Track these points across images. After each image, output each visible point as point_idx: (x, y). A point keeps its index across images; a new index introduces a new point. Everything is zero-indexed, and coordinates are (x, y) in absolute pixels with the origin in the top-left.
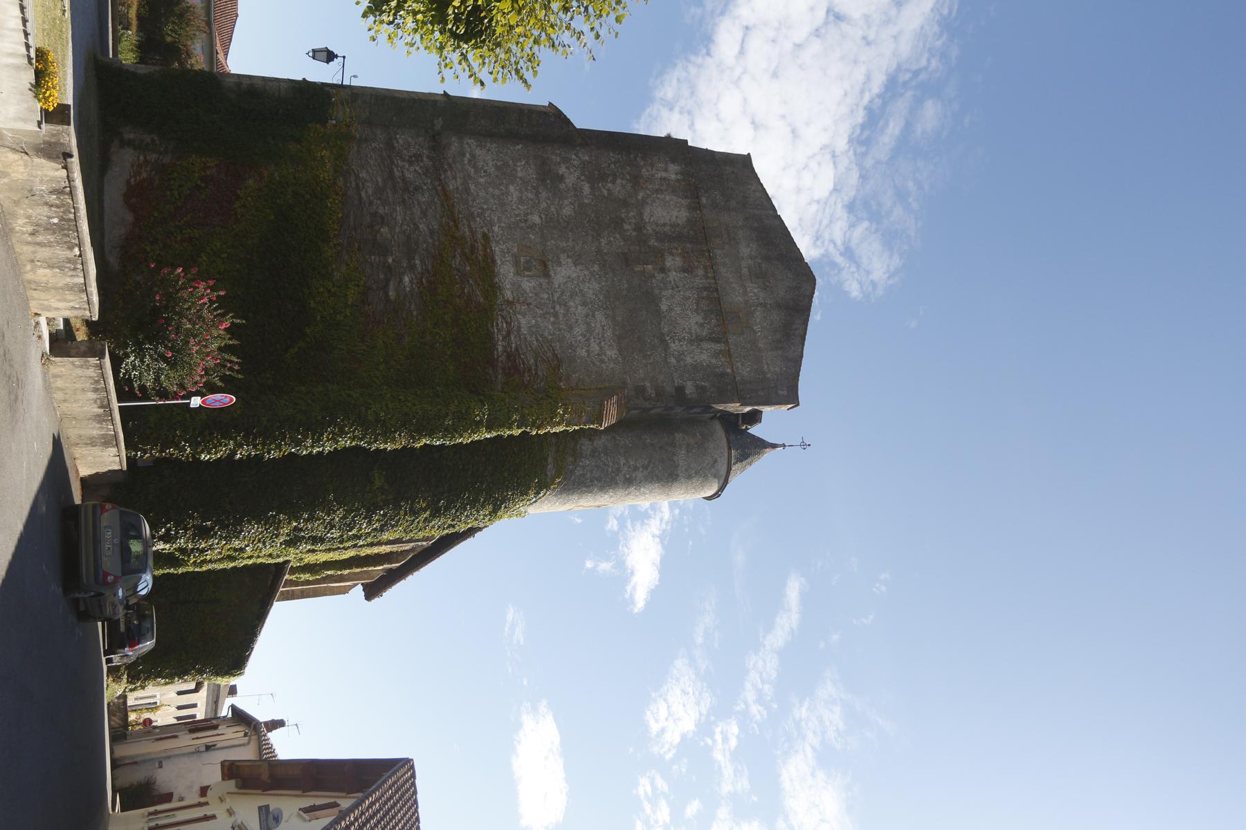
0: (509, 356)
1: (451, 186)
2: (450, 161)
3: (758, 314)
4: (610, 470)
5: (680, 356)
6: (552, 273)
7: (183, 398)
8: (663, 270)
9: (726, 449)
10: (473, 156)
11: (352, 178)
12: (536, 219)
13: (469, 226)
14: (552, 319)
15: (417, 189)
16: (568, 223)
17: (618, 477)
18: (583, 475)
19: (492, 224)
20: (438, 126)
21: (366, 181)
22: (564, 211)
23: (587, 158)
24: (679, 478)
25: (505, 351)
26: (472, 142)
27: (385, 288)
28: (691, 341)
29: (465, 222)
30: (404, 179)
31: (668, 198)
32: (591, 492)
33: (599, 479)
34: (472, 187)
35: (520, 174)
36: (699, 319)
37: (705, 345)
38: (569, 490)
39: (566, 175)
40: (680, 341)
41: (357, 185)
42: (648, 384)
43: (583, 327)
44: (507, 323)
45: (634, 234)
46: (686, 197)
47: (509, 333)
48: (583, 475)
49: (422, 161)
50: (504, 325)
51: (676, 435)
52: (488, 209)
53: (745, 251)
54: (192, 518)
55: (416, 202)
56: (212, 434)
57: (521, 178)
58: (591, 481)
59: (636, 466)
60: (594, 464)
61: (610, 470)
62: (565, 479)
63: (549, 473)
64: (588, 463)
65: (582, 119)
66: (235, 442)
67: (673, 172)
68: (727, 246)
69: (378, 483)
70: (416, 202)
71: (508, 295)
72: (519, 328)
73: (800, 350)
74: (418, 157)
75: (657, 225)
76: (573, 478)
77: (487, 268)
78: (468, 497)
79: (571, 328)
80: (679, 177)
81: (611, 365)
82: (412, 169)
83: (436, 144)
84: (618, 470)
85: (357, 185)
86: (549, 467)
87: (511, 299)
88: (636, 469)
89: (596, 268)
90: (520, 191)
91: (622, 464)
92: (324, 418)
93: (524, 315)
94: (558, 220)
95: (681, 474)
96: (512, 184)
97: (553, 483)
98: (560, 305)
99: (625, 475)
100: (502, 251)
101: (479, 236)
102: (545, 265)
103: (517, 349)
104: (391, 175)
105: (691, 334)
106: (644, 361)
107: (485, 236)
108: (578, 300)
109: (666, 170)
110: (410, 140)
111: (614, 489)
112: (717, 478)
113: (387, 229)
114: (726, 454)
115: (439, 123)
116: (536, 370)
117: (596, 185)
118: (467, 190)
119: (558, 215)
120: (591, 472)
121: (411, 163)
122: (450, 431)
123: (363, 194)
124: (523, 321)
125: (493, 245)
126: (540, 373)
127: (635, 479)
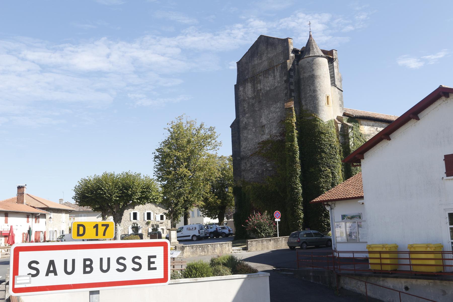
0: (281, 136)
1: (250, 154)
2: (245, 154)
3: (269, 55)
4: (311, 98)
5: (278, 82)
6: (264, 124)
7: (276, 224)
8: (261, 90)
9: (304, 59)
10: (244, 148)
11: (251, 180)
12: (254, 129)
13: (257, 148)
14: (273, 123)
15: (251, 163)
16: (254, 120)
17: (313, 95)
18: (312, 107)
19: (256, 142)
20: (239, 158)
21: (251, 176)
22: (252, 121)
23: (241, 116)
24: (313, 74)
25: (280, 137)
26: (242, 148)
27: (270, 171)
28: (275, 79)
29: (256, 150)
30: (250, 167)
31: (246, 90)
32: (318, 103)
33: (314, 101)
34: (250, 148)
35: (246, 135)
36: (270, 77)
37: (275, 74)
38: (317, 110)
39: (245, 121)
40: (275, 83)
41: (252, 179)
42: (285, 92)
43: (274, 114)
44: (274, 137)
45: (254, 100)
46: (246, 84)
47: (276, 136)
48: (312, 107)
49: (246, 162)
50: (275, 137)
51: (301, 78)
52: (253, 144)
53: (256, 62)
54: (321, 218)
55: (254, 163)
56: (295, 215)
57: (247, 135)
58: (314, 104)
59: (309, 90)
60: (309, 104)
61: (311, 98)
62: (313, 113)
63: (312, 118)
64: (309, 106)
65: (232, 117)
66: (297, 209)
67: (241, 89)
68: (256, 68)
69: (313, 170)
70: (254, 163)
71: (269, 136)
72: (275, 133)
73: (276, 39)
74: (246, 163)
75: (252, 93)
76: (313, 110)
77: (265, 143)
78: (317, 143)
79: (275, 118)
80: (242, 87)
81: (281, 104)
82: (248, 164)
83: (243, 158)
84: (311, 96)
85: (252, 179)
86: (310, 118)
87: (270, 136)
88: (310, 90)
89: (262, 111)
90: (249, 134)
91: (309, 95)
92: (290, 187)
93: (273, 132)
94: (254, 123)
95: (312, 74)
96: (248, 137)
97: (314, 116)
98: (270, 121)
99: (312, 93)
100: (261, 139)
101: (258, 146)
102: (263, 126)
103: (279, 133)
104: (249, 170)
105: (273, 79)
106: (280, 94)
107: (258, 144)
108: (269, 116)
109: (241, 91)
110: (243, 165)
111: (317, 95)
112: (313, 60)
113: (259, 171)
114: (306, 59)
115: (238, 158)
116: (283, 127)
117: (246, 112)
118: (250, 149)
119: (253, 123)
120: (311, 104)
121: (247, 165)
122: (294, 153)
123: (253, 177)
124: (274, 132)
125: (260, 141)
126: (284, 126)
127: (313, 89)
